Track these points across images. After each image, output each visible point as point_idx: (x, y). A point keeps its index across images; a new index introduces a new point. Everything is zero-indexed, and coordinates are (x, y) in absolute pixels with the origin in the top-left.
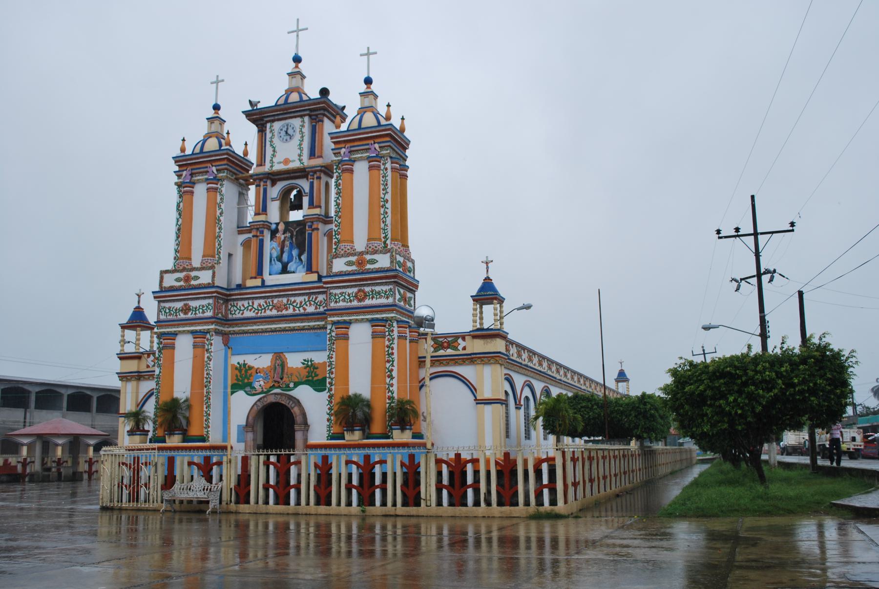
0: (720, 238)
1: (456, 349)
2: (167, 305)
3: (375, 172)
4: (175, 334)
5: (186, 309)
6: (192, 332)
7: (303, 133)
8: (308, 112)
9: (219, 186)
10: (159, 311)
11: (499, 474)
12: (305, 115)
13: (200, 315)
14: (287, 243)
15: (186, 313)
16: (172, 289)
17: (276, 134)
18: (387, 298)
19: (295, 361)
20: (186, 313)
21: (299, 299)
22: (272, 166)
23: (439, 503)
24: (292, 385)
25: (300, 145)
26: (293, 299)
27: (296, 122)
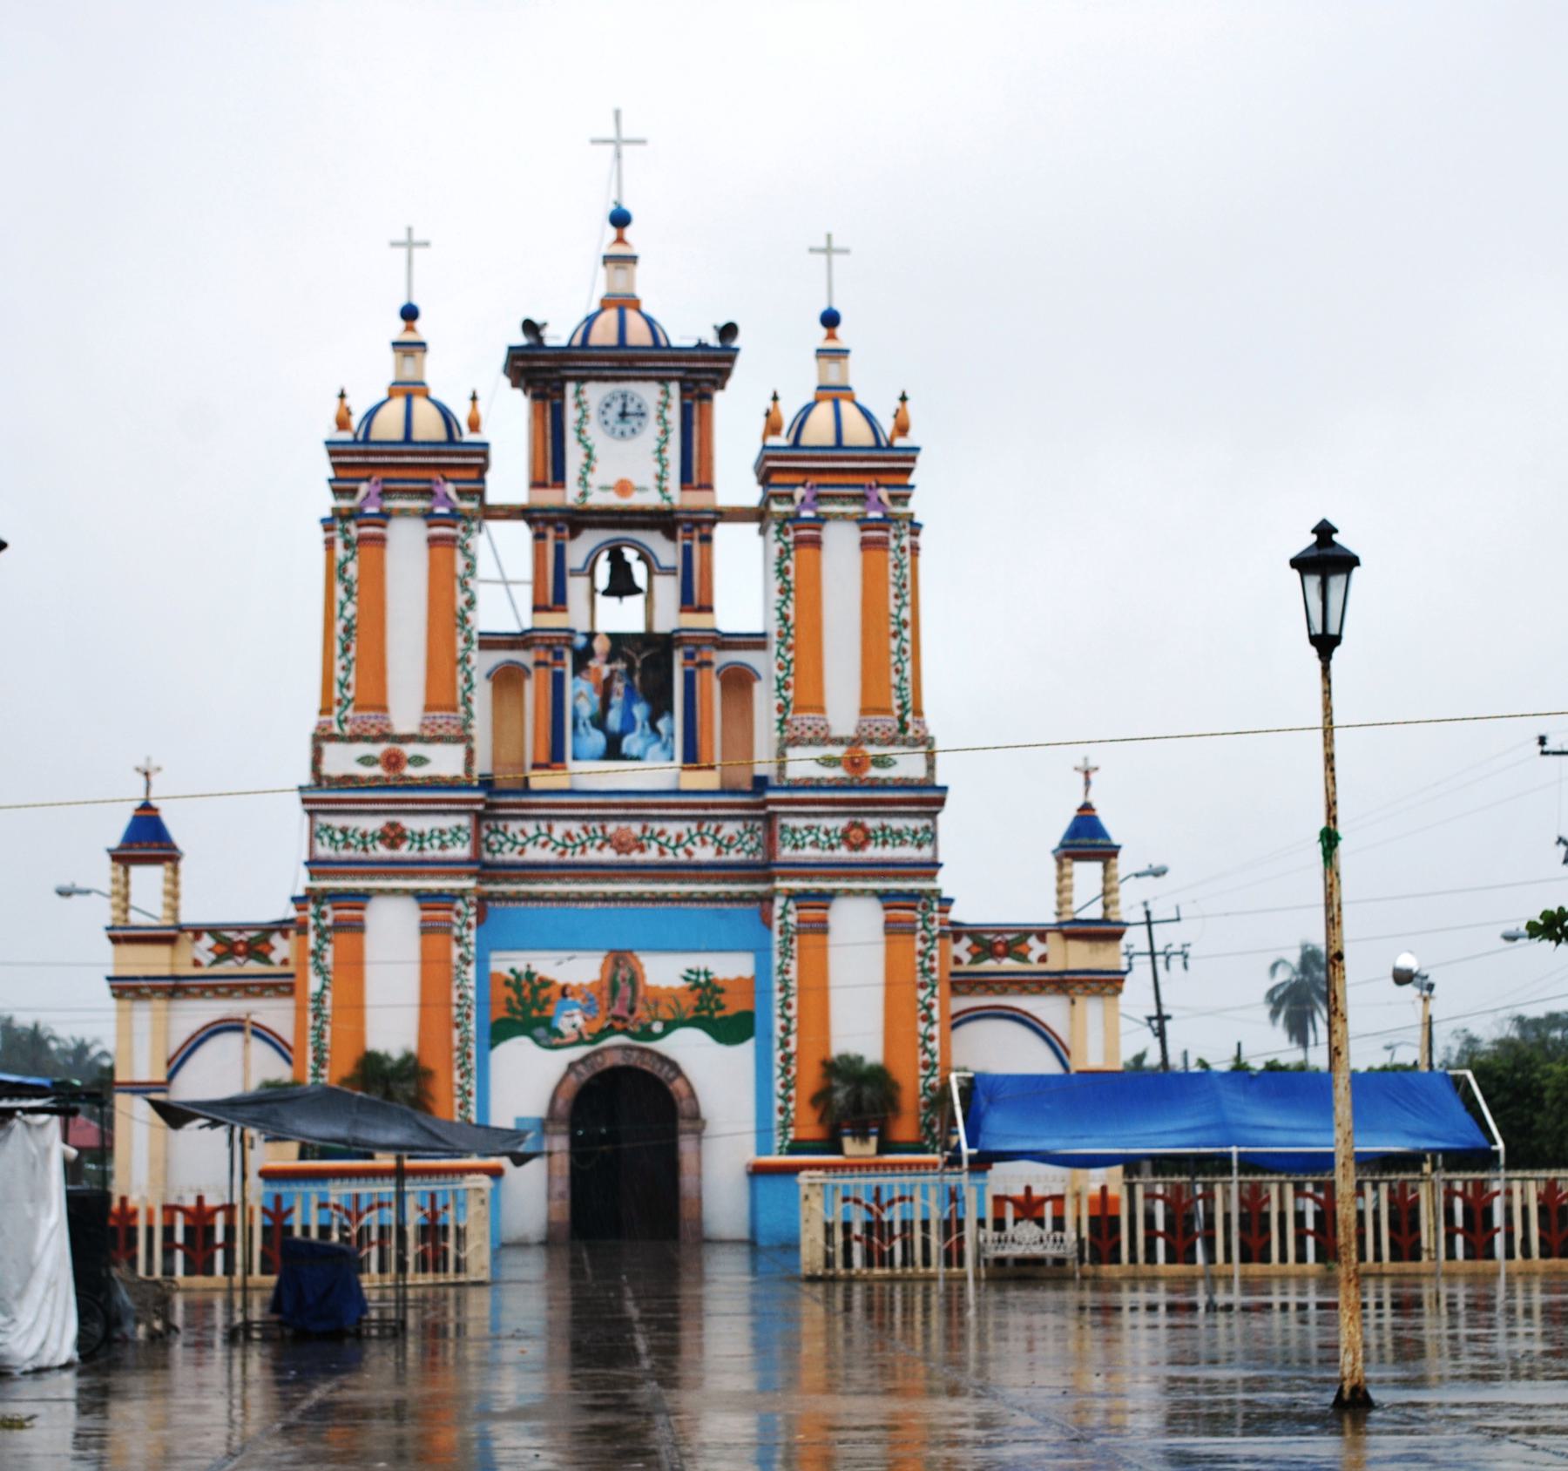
0: (1543, 753)
1: (1023, 958)
2: (337, 822)
3: (876, 554)
4: (366, 895)
5: (393, 836)
6: (418, 895)
7: (666, 423)
8: (680, 374)
9: (458, 531)
10: (314, 835)
11: (1542, 1211)
12: (671, 379)
13: (432, 852)
14: (619, 686)
15: (393, 845)
16: (347, 782)
17: (593, 412)
18: (920, 846)
19: (664, 972)
20: (393, 845)
21: (673, 829)
22: (584, 494)
23: (1451, 1255)
24: (657, 1027)
25: (660, 451)
26: (657, 826)
27: (647, 393)
